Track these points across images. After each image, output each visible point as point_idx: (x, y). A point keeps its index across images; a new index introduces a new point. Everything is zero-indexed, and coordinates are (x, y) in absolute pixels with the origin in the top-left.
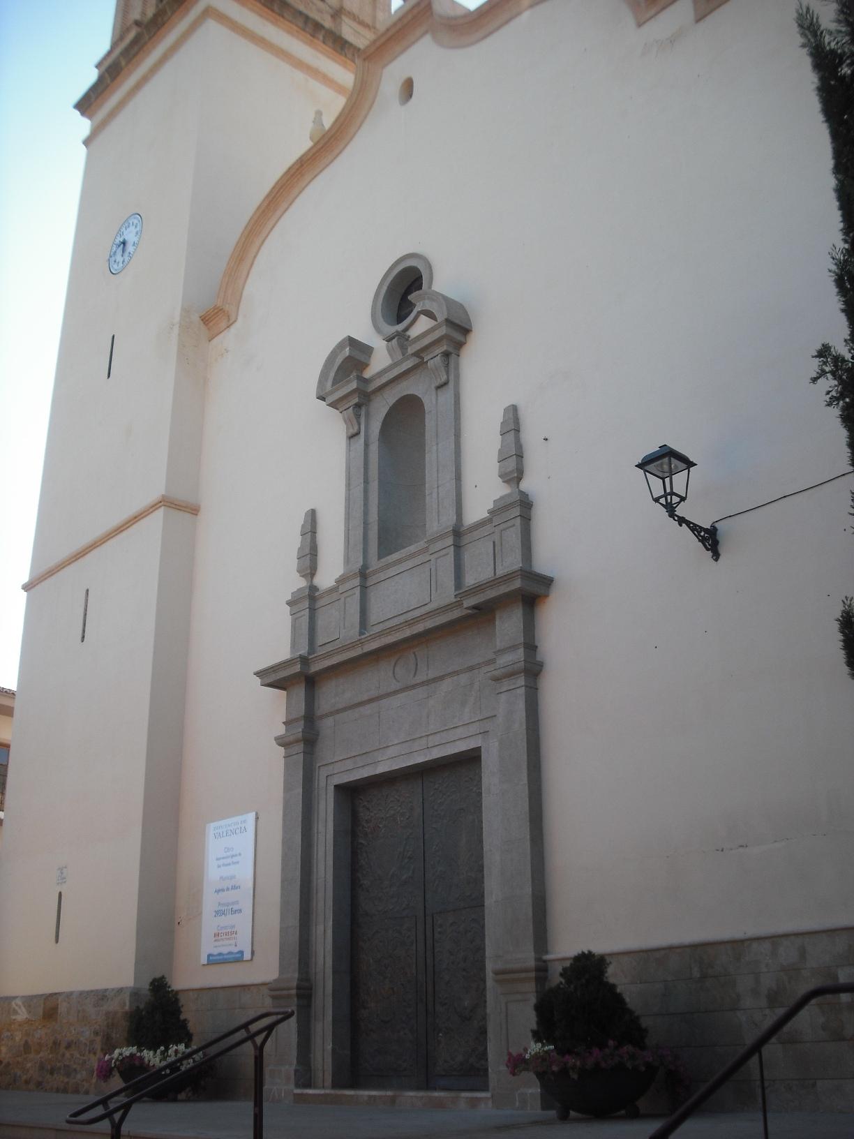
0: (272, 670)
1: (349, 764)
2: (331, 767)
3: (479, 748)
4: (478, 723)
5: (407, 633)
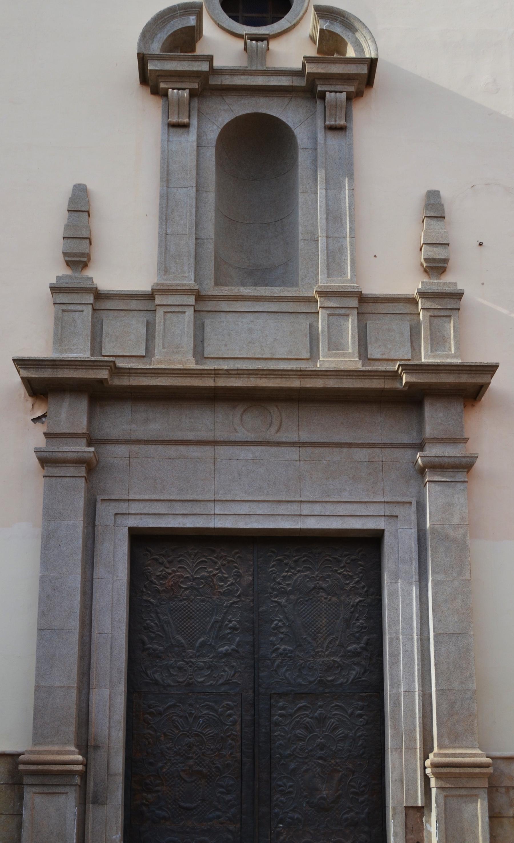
0: (52, 363)
1: (162, 508)
2: (125, 505)
3: (383, 530)
4: (382, 506)
5: (296, 383)
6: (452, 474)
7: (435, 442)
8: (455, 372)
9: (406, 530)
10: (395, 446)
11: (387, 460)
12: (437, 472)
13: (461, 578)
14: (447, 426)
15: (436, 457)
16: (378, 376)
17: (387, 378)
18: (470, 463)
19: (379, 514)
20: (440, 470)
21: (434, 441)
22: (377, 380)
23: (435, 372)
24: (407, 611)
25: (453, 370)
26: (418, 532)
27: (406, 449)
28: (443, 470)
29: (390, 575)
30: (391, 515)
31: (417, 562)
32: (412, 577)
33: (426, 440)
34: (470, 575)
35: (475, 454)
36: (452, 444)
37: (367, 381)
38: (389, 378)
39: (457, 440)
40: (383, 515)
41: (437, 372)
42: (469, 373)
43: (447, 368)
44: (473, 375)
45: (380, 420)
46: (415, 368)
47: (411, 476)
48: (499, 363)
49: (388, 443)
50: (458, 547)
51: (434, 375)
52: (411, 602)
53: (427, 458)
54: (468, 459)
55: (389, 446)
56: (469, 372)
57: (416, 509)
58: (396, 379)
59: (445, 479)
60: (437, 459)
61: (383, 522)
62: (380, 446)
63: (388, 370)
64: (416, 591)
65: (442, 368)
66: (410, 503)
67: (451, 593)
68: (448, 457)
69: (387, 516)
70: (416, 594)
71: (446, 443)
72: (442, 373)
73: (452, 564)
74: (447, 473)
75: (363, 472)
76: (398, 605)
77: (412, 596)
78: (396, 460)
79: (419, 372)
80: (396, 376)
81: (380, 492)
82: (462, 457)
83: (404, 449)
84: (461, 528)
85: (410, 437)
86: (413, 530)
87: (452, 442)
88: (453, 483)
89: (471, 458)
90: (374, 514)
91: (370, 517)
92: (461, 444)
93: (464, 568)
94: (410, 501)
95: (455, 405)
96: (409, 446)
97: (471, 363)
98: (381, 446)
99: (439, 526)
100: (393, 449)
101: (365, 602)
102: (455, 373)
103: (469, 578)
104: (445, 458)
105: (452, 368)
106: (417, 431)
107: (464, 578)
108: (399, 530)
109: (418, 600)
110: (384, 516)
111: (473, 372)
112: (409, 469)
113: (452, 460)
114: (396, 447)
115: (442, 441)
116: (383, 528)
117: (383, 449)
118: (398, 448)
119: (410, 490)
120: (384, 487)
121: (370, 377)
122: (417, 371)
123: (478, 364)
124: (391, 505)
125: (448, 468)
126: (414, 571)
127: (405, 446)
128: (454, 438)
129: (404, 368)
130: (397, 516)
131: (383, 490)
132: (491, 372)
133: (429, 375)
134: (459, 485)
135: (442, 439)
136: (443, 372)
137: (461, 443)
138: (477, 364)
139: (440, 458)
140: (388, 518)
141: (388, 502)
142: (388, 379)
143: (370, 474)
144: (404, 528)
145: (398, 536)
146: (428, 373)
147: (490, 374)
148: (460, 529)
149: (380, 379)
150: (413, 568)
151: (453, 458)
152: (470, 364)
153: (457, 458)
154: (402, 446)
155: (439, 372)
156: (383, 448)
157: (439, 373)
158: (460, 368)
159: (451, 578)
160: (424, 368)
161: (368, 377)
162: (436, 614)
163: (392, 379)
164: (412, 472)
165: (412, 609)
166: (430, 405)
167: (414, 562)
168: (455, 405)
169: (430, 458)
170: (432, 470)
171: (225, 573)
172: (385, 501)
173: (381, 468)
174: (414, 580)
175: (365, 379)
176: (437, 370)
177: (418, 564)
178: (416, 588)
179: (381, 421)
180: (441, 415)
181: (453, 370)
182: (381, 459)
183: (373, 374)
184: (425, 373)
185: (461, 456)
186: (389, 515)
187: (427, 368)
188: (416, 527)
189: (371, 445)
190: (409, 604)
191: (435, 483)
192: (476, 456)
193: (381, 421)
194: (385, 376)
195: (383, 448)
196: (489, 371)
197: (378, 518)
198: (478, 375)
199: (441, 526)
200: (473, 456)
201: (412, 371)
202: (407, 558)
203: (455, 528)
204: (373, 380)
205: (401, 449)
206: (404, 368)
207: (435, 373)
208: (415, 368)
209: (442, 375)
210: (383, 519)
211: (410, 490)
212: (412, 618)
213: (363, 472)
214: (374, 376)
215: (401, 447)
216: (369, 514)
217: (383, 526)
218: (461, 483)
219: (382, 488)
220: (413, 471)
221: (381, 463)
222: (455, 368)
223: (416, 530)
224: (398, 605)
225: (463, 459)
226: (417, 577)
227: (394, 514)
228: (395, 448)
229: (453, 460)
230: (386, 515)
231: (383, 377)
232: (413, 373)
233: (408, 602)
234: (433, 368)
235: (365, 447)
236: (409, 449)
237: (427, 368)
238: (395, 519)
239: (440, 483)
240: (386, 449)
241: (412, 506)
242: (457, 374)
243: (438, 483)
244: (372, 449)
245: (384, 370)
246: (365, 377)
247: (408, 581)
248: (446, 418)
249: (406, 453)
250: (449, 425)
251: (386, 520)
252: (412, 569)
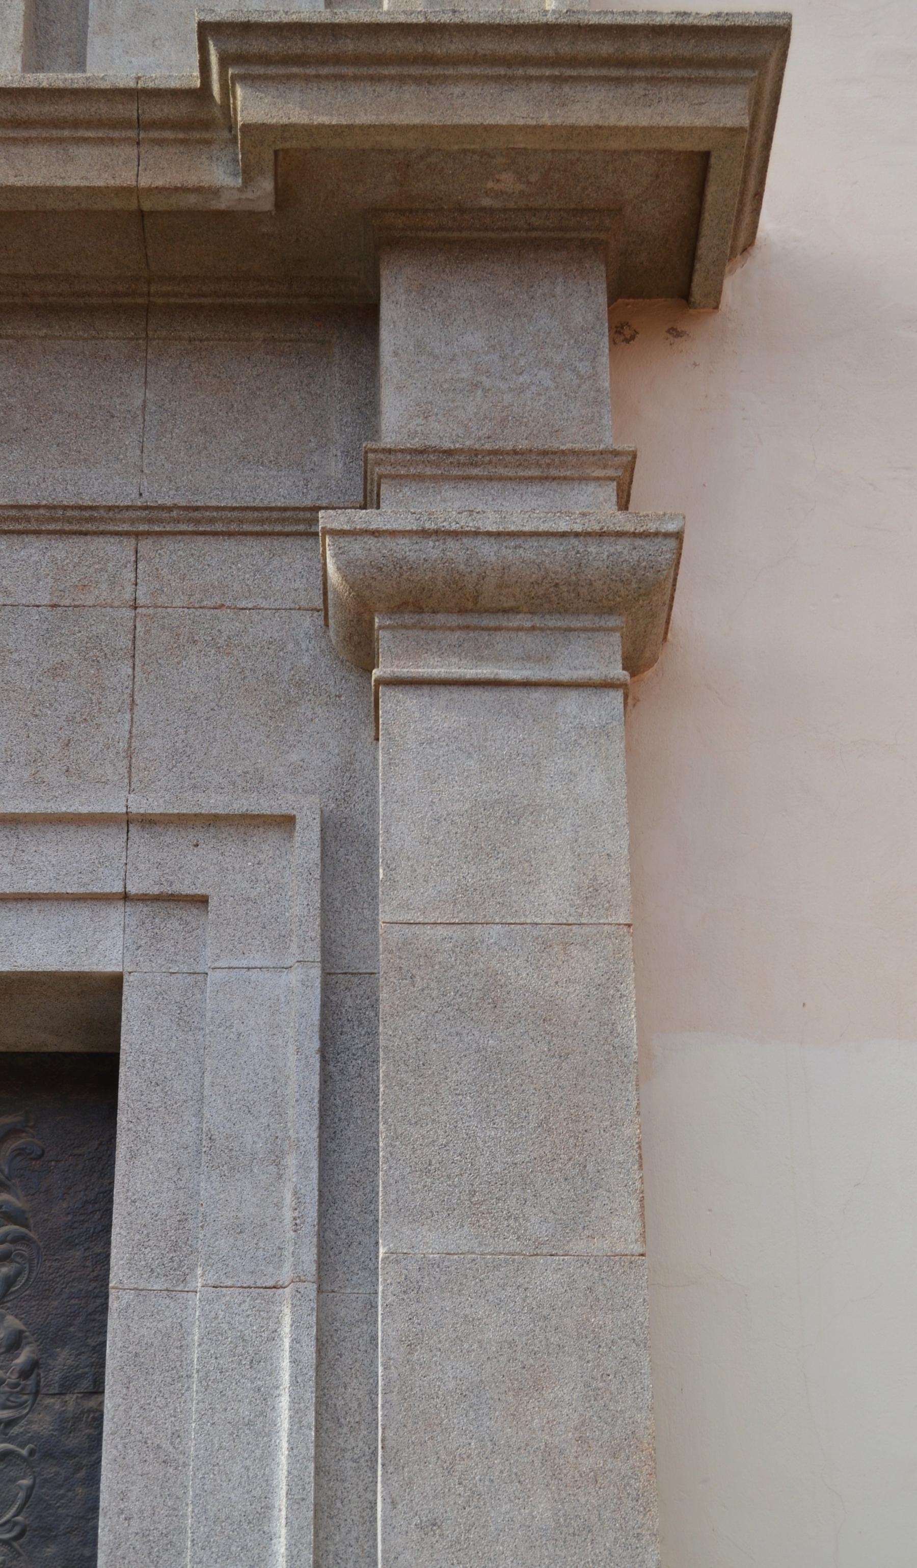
6: (531, 642)
7: (434, 478)
8: (532, 71)
9: (254, 975)
10: (212, 521)
11: (161, 600)
12: (440, 635)
13: (579, 1246)
14: (508, 398)
15: (425, 533)
16: (100, 124)
17: (155, 134)
18: (634, 570)
19: (95, 889)
20: (455, 620)
21: (428, 471)
22: (96, 152)
23: (415, 71)
24: (237, 1469)
25: (526, 61)
26: (327, 988)
27: (276, 542)
28: (472, 620)
29: (140, 1244)
30: (167, 889)
31: (314, 1164)
32: (276, 1257)
33: (378, 463)
34: (637, 1227)
35: (661, 518)
36: (537, 488)
37: (37, 153)
38: (168, 134)
39: (563, 464)
40: (118, 888)
41: (430, 71)
42: (617, 81)
43: (487, 46)
44: (639, 89)
45: (138, 402)
46: (296, 47)
47: (299, 685)
48: (790, 17)
49: (169, 502)
50: (564, 1057)
51: (409, 92)
52: (262, 1413)
53: (371, 541)
54: (622, 546)
55: (178, 521)
56: (621, 72)
57: (316, 855)
58: (208, 142)
59: (486, 671)
60: (432, 550)
61: (119, 930)
62: (126, 527)
63: (151, 85)
64: (295, 1341)
65: (456, 46)
66: (286, 822)
67: (512, 1344)
68: (499, 534)
69: (144, 898)
70: (294, 1362)
71: (501, 479)
72: (457, 79)
73: (519, 1158)
74: (499, 636)
75: (18, 663)
76: (176, 1435)
77: (273, 1372)
78: (217, 600)
79: (325, 71)
80: (206, 125)
81: (109, 770)
82: (588, 534)
83: (266, 541)
84: (584, 945)
85: (307, 481)
86: (293, 978)
87: (535, 472)
88: (537, 695)
89: (639, 542)
90: (58, 888)
91: (35, 907)
92: (591, 487)
93: (598, 1186)
94: (285, 810)
95: (559, 290)
96: (298, 521)
97: (623, 13)
98: (133, 521)
99: (442, 931)
100: (201, 539)
101: (15, 1430)
102: (539, 79)
103: (637, 1248)
104: (478, 542)
105: (514, 47)
106: (346, 453)
107: (600, 1246)
108: (213, 976)
109: (310, 1396)
110: (125, 897)
111: (638, 73)
112: (290, 646)
113: (529, 551)
114: (219, 527)
115: (475, 471)
116: (118, 969)
117: (146, 545)
118: (230, 534)
119: (294, 757)
120: (136, 744)
121: (55, 133)
122: (311, 71)
123: (667, 20)
124: (170, 836)
125: (505, 611)
126: (288, 1215)
127: (269, 520)
128: (545, 453)
129: (233, 46)
130: (202, 901)
131: (130, 754)
132: (748, 73)
133: (380, 89)
134: (571, 702)
135: (474, 456)
136: (464, 70)
137: (584, 479)
138: (658, 20)
139: (451, 543)
140: (144, 909)
141: (148, 821)
142: (161, 142)
143: (55, 672)
144: (245, 963)
145: (203, 1016)
146: (380, 79)
147: (744, 81)
148: (575, 951)
149: (112, 141)
150: (288, 1198)
151: (533, 542)
152: (620, 20)
153: (552, 543)
154: (254, 521)
155: (438, 71)
156: (148, 534)
157: (444, 79)
158: (564, 47)
159: (516, 1246)
160: (349, 46)
161: (44, 134)
162: (410, 1483)
163: (183, 142)
164: (306, 660)
165: (267, 1456)
166: (408, 291)
167: (291, 1161)
168: (559, 290)
169: (390, 543)
170: (409, 619)
171: (13, 1519)
172: (134, 809)
173: (124, 642)
174: (286, 1273)
175: (27, 141)
176: (429, 60)
177: (314, 1175)
178: (296, 1324)
179: (144, 406)
180: (475, 340)
181: (526, 61)
182: (128, 596)
183: (66, 109)
184: (356, 78)
185: (578, 528)
186: (156, 890)
187: (365, 46)
188: (317, 955)
189: (69, 521)
190: (249, 1424)
191: (426, 690)
192: (671, 527)
193: (144, 406)
194: (140, 125)
195: (148, 534)
196: (734, 63)
197: (84, 913)
198: (669, 91)
199: (457, 933)
200: (652, 527)
201: (282, 71)
202: (249, 1139)
203: (546, 945)
204: (74, 150)
205: (249, 541)
206: (233, 46)
207: (418, 80)
208: (296, 47)
209: (457, 90)
210: (116, 915)
211: (294, 757)
212: (265, 1512)
213: (18, 663)
214: (76, 124)
215: (246, 527)
216: (30, 886)
217: (117, 954)
218: (585, 693)
219: (123, 745)
220: (315, 658)
221: (128, 613)
222: (532, 48)
223: (316, 972)
224: (176, 1435)
225: (592, 549)
226: (309, 1256)
227: (186, 888)
228: (215, 534)
229: (529, 555)
230: (132, 889)
231: (131, 134)
232: (289, 77)
233: (245, 1411)
234: (403, 45)
235: (37, 533)
236: (298, 541)
237: (365, 46)
238: (191, 914)
239: (457, 694)
240: (164, 541)
241: (297, 838)
242: (546, 87)
243: (444, 694)
244: (81, 541)
245: (132, 84)
246: (24, 134)
247: (248, 1280)
248: (503, 358)
249: (276, 562)
250: (522, 390)
251: (133, 922)
252: (278, 1206)
